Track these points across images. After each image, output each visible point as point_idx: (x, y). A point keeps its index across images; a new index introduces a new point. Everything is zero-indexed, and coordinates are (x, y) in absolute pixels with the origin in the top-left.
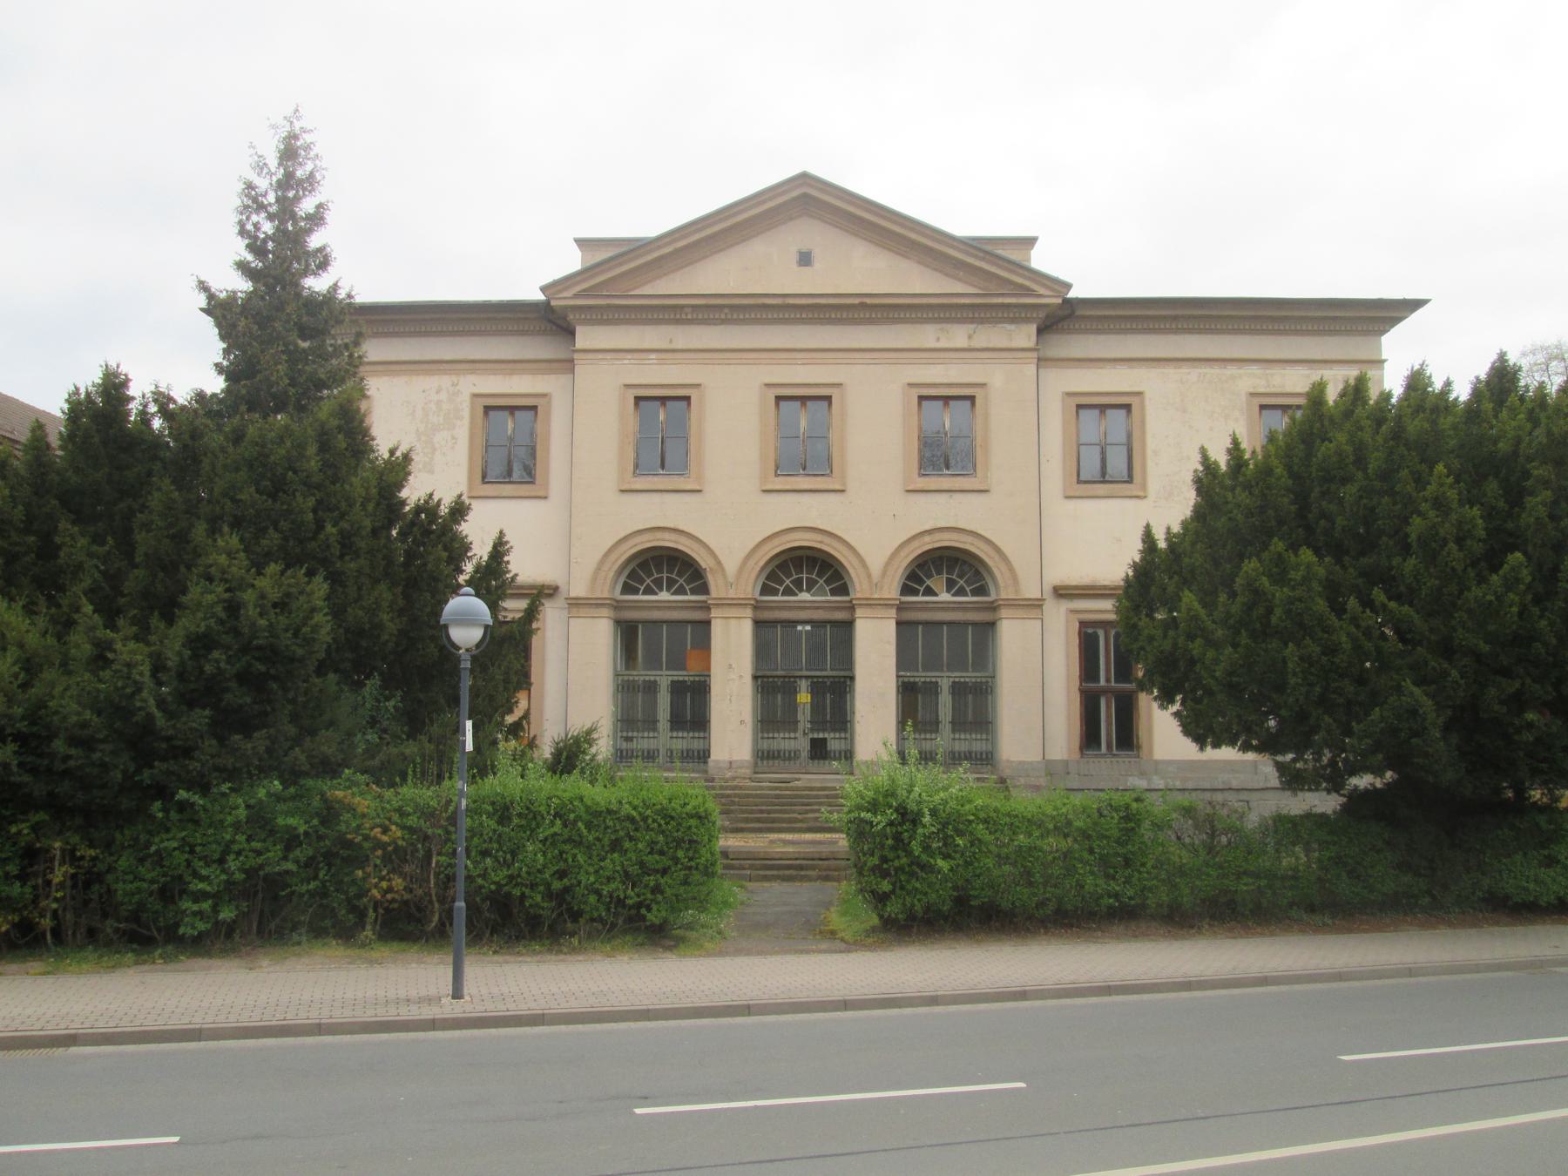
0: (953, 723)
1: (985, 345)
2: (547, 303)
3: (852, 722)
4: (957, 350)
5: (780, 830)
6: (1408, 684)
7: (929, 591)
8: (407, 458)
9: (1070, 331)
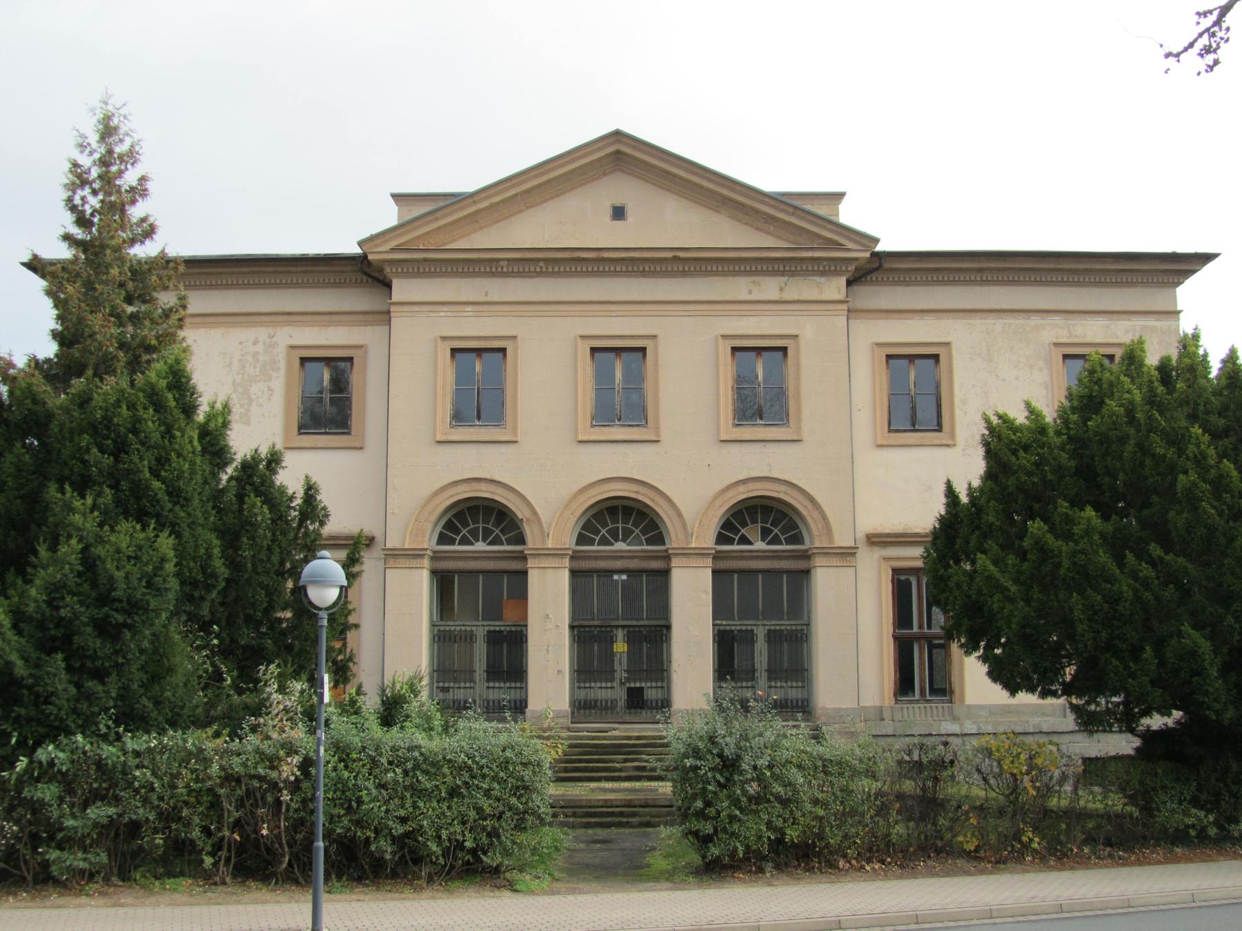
0: (769, 671)
1: (796, 297)
2: (364, 257)
3: (668, 671)
4: (768, 302)
5: (599, 779)
6: (1187, 628)
7: (744, 540)
8: (227, 407)
9: (872, 283)
